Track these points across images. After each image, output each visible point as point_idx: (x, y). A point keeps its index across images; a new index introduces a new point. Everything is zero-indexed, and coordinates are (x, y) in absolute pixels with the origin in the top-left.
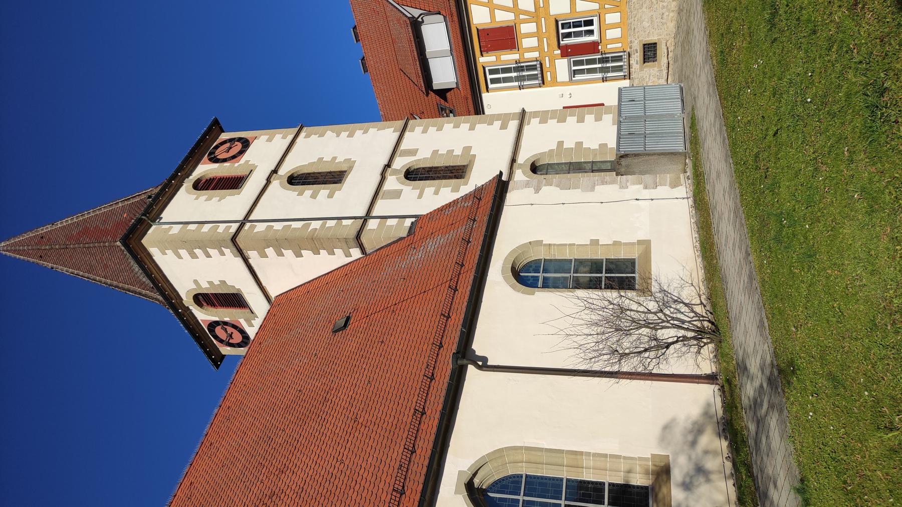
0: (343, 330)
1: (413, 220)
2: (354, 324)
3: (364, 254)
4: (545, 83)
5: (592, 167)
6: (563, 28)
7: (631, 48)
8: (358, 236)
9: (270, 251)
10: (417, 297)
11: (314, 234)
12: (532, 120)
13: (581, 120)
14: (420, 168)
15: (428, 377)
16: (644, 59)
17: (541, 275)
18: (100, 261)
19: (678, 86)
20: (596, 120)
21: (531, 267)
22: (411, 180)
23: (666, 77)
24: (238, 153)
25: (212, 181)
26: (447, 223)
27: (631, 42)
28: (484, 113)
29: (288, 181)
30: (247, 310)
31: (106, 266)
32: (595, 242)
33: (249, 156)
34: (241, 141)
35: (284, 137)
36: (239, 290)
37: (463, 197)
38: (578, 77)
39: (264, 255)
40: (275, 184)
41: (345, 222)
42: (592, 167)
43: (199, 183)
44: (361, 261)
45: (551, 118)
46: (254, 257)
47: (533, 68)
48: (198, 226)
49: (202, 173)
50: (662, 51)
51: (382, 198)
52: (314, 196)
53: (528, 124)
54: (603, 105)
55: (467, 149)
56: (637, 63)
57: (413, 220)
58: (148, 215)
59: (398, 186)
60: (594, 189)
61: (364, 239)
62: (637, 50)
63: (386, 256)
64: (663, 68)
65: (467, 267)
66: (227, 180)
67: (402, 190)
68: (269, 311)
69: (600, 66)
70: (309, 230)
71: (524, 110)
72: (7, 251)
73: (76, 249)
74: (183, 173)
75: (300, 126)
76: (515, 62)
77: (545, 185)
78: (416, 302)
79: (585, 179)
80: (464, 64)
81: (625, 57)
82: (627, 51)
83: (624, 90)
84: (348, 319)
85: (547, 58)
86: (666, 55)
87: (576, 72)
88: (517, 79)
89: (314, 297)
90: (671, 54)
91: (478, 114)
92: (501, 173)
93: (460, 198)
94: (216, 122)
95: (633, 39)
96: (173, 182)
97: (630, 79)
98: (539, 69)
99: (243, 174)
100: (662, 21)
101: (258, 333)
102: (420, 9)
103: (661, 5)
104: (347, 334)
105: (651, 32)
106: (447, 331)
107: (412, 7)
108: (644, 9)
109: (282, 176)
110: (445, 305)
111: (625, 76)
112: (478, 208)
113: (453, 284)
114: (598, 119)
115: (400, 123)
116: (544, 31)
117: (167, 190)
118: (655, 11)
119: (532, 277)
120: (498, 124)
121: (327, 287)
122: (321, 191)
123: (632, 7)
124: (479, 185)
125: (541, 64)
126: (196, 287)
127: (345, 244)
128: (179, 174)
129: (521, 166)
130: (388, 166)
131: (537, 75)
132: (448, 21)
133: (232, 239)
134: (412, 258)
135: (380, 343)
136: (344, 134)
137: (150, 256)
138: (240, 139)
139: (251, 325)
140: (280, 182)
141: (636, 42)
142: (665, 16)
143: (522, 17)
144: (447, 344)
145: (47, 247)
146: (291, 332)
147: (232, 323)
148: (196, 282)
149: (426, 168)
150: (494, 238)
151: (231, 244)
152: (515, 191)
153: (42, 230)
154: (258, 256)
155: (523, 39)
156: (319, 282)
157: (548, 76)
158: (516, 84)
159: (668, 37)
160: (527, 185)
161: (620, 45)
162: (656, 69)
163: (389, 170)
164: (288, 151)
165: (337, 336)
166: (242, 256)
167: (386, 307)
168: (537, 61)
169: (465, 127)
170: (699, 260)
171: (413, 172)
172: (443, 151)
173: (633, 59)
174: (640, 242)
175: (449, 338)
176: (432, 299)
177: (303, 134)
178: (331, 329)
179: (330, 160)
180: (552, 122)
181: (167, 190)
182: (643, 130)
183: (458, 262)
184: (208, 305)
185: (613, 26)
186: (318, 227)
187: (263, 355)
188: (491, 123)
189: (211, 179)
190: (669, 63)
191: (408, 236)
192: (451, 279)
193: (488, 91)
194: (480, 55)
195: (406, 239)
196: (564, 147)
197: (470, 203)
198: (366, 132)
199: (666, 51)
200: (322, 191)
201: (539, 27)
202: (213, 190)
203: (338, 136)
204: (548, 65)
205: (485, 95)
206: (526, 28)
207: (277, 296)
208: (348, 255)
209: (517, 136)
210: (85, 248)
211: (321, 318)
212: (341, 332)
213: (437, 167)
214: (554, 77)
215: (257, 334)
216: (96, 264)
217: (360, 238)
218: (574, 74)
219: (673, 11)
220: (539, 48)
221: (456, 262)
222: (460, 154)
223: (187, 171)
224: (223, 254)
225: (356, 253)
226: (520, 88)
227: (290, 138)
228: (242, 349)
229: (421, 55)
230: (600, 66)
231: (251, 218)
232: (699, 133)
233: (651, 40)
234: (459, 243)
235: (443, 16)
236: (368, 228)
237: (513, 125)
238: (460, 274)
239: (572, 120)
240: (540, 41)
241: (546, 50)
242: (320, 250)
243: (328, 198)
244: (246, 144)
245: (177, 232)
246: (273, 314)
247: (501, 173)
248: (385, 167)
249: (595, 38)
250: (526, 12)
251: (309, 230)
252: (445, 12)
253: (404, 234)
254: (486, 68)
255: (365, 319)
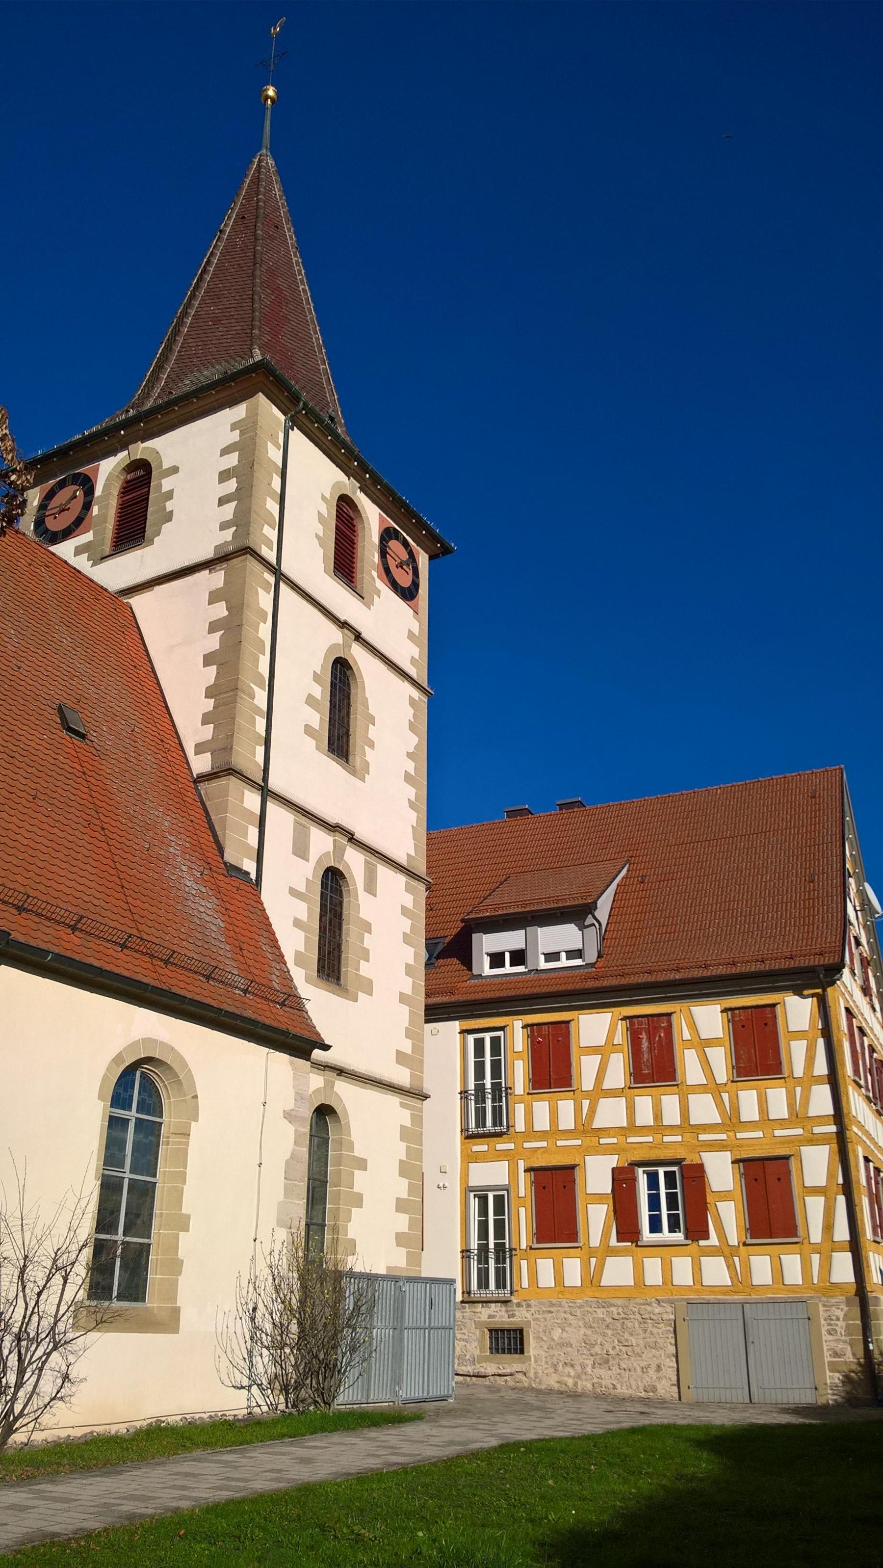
0: (62, 724)
1: (253, 876)
2: (71, 745)
3: (198, 778)
4: (467, 1141)
5: (314, 1224)
7: (519, 1305)
8: (231, 771)
9: (220, 610)
10: (113, 872)
11: (243, 692)
12: (407, 1113)
13: (401, 1206)
14: (341, 896)
15: (125, 942)
16: (496, 1331)
17: (133, 1114)
18: (227, 314)
19: (450, 1392)
20: (398, 1235)
21: (150, 1096)
22: (323, 877)
23: (461, 1373)
24: (394, 580)
25: (352, 529)
26: (244, 939)
27: (529, 1306)
28: (427, 1021)
29: (340, 658)
30: (108, 550)
31: (216, 321)
32: (184, 1224)
33: (387, 597)
34: (412, 587)
35: (413, 661)
36: (151, 542)
37: (289, 972)
38: (474, 1204)
39: (214, 597)
40: (336, 635)
41: (260, 750)
42: (314, 1224)
43: (347, 504)
44: (185, 771)
45: (408, 1149)
46: (216, 579)
47: (497, 1120)
48: (275, 492)
49: (366, 513)
50: (510, 1364)
51: (296, 822)
52: (310, 701)
53: (403, 1105)
54: (423, 1250)
55: (368, 987)
56: (490, 1317)
57: (253, 876)
58: (304, 412)
59: (315, 853)
60: (281, 1227)
61: (233, 782)
62: (513, 1316)
63: (192, 818)
64: (478, 1366)
65: (162, 971)
66: (350, 553)
67: (308, 860)
68: (106, 590)
69: (491, 1246)
70: (252, 685)
71: (427, 1098)
72: (259, 166)
73: (251, 278)
74: (369, 482)
75: (430, 691)
76: (509, 1085)
77: (296, 1131)
78: (104, 868)
79: (299, 1208)
80: (512, 993)
81: (504, 1294)
82: (513, 1298)
83: (450, 1289)
84: (83, 736)
85: (512, 1146)
86: (500, 1372)
87: (483, 1200)
88: (480, 1089)
89: (125, 677)
90: (500, 1381)
91: (426, 1010)
92: (327, 1048)
93: (288, 969)
94: (446, 551)
95: (532, 1310)
96: (356, 463)
97: (462, 1302)
98: (492, 1130)
99: (358, 582)
100: (561, 1364)
101: (68, 564)
102: (608, 923)
103: (588, 1361)
104: (54, 731)
105: (542, 1343)
106: (49, 924)
107: (612, 908)
108: (583, 1330)
109: (350, 651)
110: (107, 928)
111: (469, 1293)
112: (266, 999)
113: (133, 943)
114: (401, 1239)
115: (421, 868)
116: (559, 1143)
117: (329, 438)
118: (578, 1351)
119: (131, 1097)
120: (407, 1046)
121: (143, 703)
122: (319, 715)
123: (589, 1309)
124: (308, 1006)
125: (499, 1135)
126: (164, 468)
127: (221, 747)
128: (367, 476)
129: (329, 1085)
130: (352, 838)
131: (484, 1126)
132: (586, 970)
133: (249, 548)
134: (184, 868)
135: (33, 793)
136: (410, 766)
137: (232, 402)
138: (416, 585)
139: (78, 551)
140: (339, 644)
141: (528, 1315)
142: (569, 1369)
143: (586, 1103)
144: (24, 922)
145: (259, 232)
146: (65, 627)
147: (86, 519)
148: (175, 470)
149: (341, 908)
150: (170, 1013)
151: (240, 544)
152: (292, 1073)
153: (289, 230)
154: (214, 588)
155: (547, 1102)
156: (152, 688)
157: (480, 1147)
158: (471, 1086)
159: (531, 1374)
160: (300, 1097)
161: (525, 1284)
162: (477, 1352)
163: (343, 841)
164: (389, 665)
165: (53, 712)
166: (218, 559)
167: (100, 810)
168: (508, 1127)
169: (406, 985)
170: (78, 1433)
171: (337, 883)
172: (369, 941)
173: (498, 1309)
174: (176, 1311)
175: (35, 926)
176: (108, 899)
177: (416, 694)
178: (66, 701)
179: (369, 736)
180: (400, 1150)
181: (316, 425)
182: (379, 1324)
183: (83, 921)
184: (128, 482)
186: (256, 701)
187: (26, 569)
188: (409, 1034)
189: (354, 526)
190: (484, 1377)
191: (225, 863)
192: (142, 939)
193: (462, 1032)
194: (525, 1023)
195: (220, 860)
196: (356, 1171)
197: (276, 985)
198: (412, 805)
199: (508, 1371)
200: (318, 716)
202: (336, 528)
203: (409, 755)
204: (500, 1147)
205: (456, 1026)
206: (566, 1108)
207: (131, 608)
208: (200, 749)
209: (384, 1082)
210: (253, 295)
211: (87, 685)
212: (59, 721)
213: (340, 928)
214: (477, 1158)
215: (65, 562)
216: (223, 307)
217: (230, 774)
218: (480, 1197)
219: (576, 1384)
220: (531, 1133)
221: (174, 952)
222: (361, 973)
223: (372, 489)
224: (224, 526)
225: (201, 764)
226: (464, 1093)
227: (412, 671)
228: (32, 528)
229: (532, 917)
230: (491, 1246)
231: (283, 586)
233: (529, 1344)
234: (207, 960)
235: (594, 962)
236: (246, 792)
237: (402, 1076)
238: (152, 956)
239: (402, 1188)
240: (543, 1135)
241: (526, 1145)
242: (213, 700)
243: (306, 726)
244: (408, 594)
245: (269, 455)
246: (100, 597)
247: (327, 1048)
248: (351, 834)
250: (592, 1110)
251: (252, 685)
252: (601, 965)
253: (230, 856)
254: (502, 1032)
255: (79, 767)
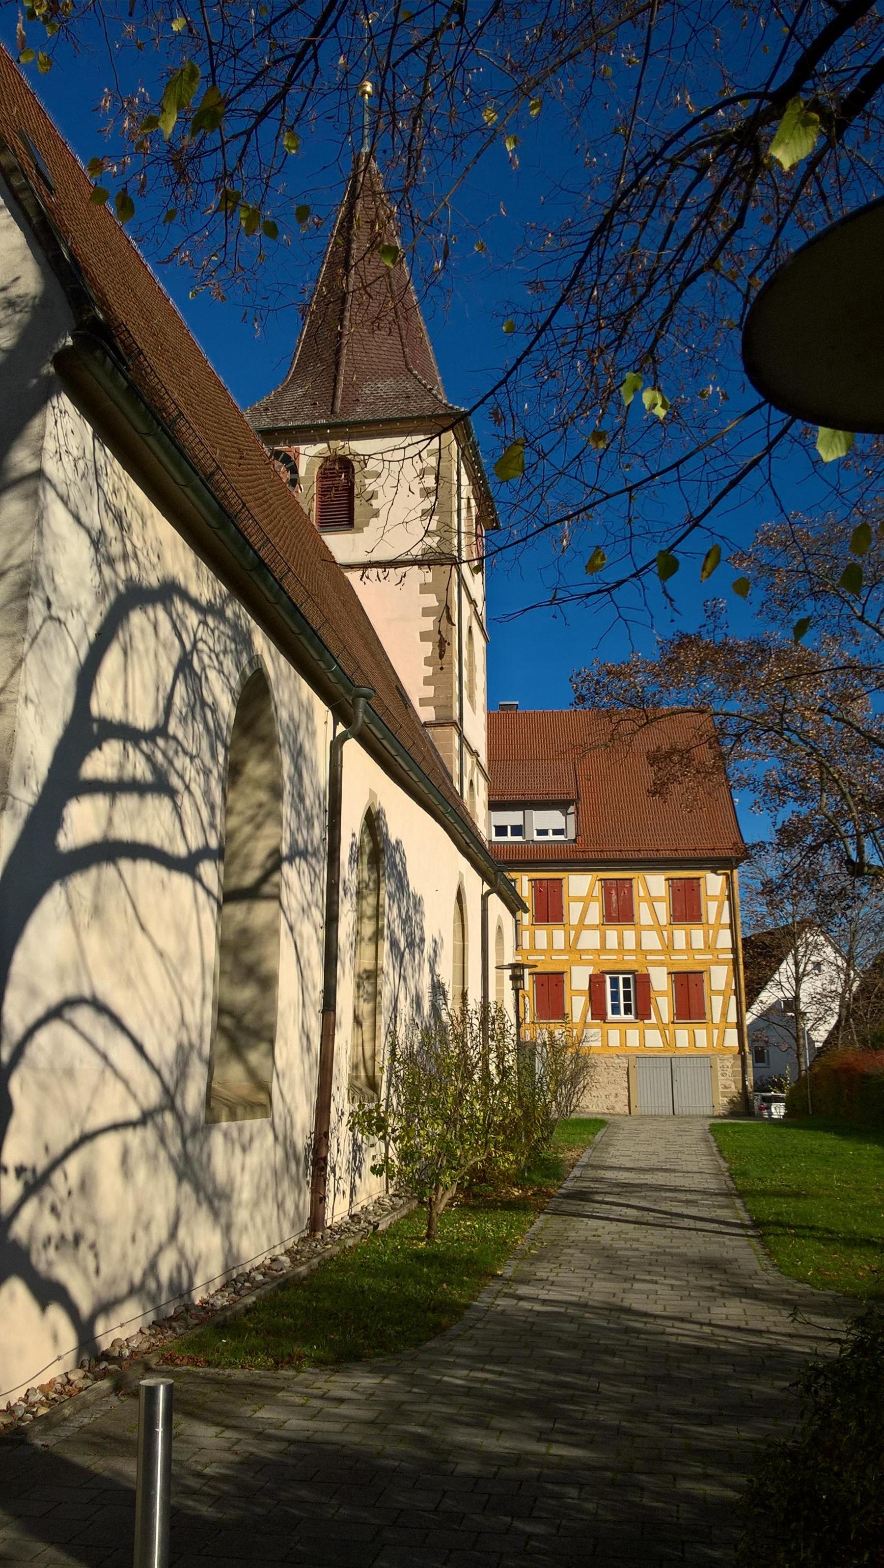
6: (624, 979)
116: (553, 957)
143: (573, 933)
185: (624, 1037)
201: (560, 952)
206: (559, 935)
232: (761, 1252)
240: (543, 952)
249: (610, 1016)
250: (577, 938)
